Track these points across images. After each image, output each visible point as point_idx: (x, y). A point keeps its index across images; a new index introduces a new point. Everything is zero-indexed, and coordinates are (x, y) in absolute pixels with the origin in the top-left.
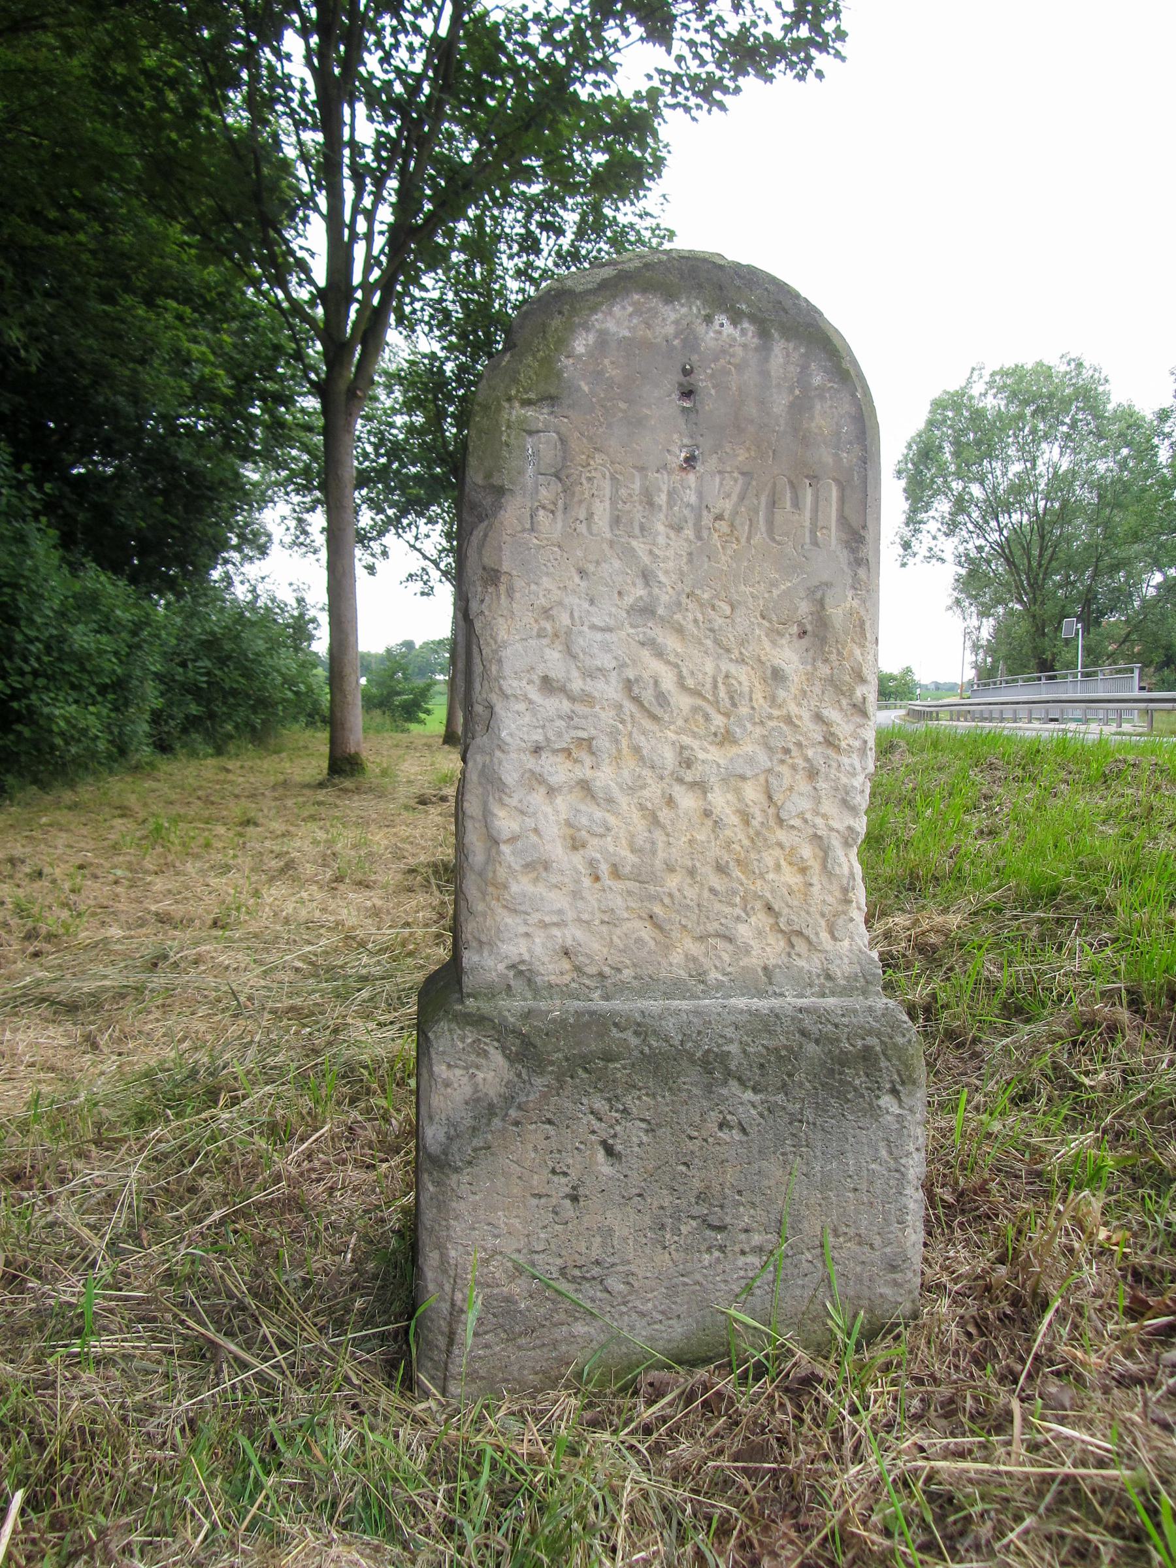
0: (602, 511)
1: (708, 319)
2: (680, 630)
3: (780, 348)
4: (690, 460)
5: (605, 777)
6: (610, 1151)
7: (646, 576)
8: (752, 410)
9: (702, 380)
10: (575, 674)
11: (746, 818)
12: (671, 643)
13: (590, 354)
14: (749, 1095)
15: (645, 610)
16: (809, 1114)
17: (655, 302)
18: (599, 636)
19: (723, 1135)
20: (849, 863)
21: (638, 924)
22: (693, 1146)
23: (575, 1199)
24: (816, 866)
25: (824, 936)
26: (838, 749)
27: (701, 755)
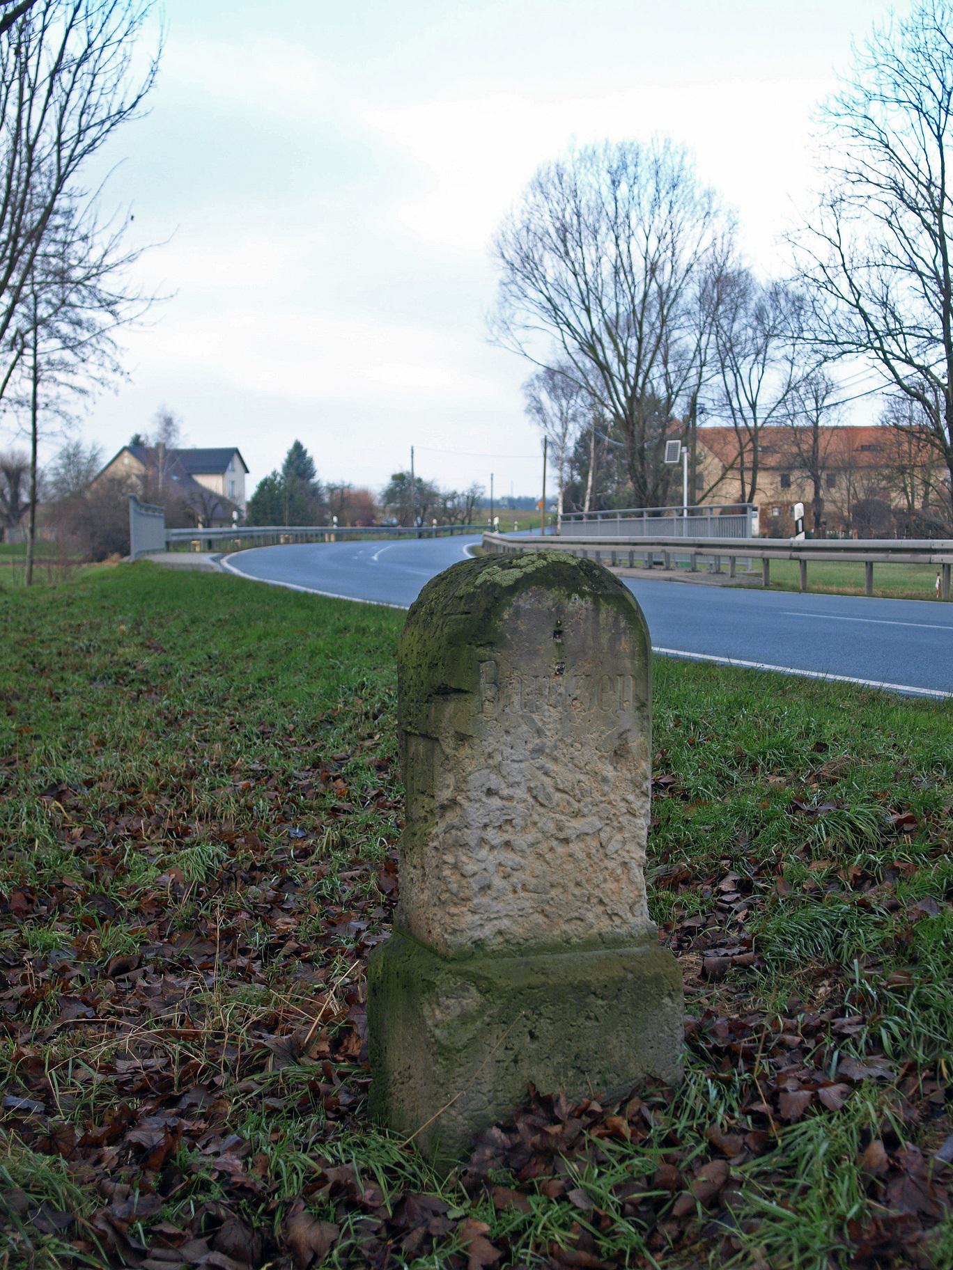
0: (516, 699)
1: (569, 596)
2: (555, 760)
3: (604, 608)
4: (560, 671)
5: (521, 841)
6: (532, 1036)
7: (539, 732)
8: (590, 642)
9: (567, 629)
10: (504, 786)
11: (589, 856)
12: (550, 766)
13: (510, 619)
14: (600, 1002)
15: (539, 751)
16: (629, 1010)
17: (543, 590)
18: (516, 765)
19: (588, 1024)
20: (638, 874)
21: (536, 915)
22: (572, 1030)
23: (515, 1061)
24: (624, 877)
25: (629, 915)
26: (634, 815)
27: (567, 824)
